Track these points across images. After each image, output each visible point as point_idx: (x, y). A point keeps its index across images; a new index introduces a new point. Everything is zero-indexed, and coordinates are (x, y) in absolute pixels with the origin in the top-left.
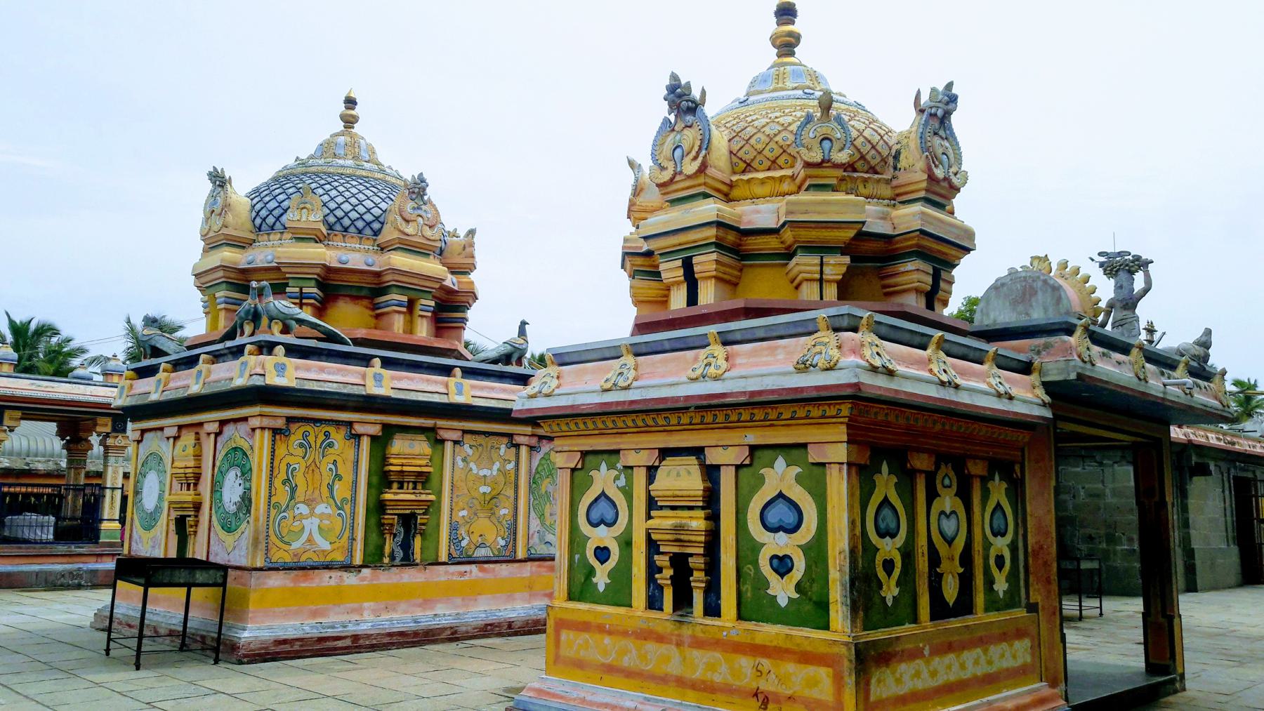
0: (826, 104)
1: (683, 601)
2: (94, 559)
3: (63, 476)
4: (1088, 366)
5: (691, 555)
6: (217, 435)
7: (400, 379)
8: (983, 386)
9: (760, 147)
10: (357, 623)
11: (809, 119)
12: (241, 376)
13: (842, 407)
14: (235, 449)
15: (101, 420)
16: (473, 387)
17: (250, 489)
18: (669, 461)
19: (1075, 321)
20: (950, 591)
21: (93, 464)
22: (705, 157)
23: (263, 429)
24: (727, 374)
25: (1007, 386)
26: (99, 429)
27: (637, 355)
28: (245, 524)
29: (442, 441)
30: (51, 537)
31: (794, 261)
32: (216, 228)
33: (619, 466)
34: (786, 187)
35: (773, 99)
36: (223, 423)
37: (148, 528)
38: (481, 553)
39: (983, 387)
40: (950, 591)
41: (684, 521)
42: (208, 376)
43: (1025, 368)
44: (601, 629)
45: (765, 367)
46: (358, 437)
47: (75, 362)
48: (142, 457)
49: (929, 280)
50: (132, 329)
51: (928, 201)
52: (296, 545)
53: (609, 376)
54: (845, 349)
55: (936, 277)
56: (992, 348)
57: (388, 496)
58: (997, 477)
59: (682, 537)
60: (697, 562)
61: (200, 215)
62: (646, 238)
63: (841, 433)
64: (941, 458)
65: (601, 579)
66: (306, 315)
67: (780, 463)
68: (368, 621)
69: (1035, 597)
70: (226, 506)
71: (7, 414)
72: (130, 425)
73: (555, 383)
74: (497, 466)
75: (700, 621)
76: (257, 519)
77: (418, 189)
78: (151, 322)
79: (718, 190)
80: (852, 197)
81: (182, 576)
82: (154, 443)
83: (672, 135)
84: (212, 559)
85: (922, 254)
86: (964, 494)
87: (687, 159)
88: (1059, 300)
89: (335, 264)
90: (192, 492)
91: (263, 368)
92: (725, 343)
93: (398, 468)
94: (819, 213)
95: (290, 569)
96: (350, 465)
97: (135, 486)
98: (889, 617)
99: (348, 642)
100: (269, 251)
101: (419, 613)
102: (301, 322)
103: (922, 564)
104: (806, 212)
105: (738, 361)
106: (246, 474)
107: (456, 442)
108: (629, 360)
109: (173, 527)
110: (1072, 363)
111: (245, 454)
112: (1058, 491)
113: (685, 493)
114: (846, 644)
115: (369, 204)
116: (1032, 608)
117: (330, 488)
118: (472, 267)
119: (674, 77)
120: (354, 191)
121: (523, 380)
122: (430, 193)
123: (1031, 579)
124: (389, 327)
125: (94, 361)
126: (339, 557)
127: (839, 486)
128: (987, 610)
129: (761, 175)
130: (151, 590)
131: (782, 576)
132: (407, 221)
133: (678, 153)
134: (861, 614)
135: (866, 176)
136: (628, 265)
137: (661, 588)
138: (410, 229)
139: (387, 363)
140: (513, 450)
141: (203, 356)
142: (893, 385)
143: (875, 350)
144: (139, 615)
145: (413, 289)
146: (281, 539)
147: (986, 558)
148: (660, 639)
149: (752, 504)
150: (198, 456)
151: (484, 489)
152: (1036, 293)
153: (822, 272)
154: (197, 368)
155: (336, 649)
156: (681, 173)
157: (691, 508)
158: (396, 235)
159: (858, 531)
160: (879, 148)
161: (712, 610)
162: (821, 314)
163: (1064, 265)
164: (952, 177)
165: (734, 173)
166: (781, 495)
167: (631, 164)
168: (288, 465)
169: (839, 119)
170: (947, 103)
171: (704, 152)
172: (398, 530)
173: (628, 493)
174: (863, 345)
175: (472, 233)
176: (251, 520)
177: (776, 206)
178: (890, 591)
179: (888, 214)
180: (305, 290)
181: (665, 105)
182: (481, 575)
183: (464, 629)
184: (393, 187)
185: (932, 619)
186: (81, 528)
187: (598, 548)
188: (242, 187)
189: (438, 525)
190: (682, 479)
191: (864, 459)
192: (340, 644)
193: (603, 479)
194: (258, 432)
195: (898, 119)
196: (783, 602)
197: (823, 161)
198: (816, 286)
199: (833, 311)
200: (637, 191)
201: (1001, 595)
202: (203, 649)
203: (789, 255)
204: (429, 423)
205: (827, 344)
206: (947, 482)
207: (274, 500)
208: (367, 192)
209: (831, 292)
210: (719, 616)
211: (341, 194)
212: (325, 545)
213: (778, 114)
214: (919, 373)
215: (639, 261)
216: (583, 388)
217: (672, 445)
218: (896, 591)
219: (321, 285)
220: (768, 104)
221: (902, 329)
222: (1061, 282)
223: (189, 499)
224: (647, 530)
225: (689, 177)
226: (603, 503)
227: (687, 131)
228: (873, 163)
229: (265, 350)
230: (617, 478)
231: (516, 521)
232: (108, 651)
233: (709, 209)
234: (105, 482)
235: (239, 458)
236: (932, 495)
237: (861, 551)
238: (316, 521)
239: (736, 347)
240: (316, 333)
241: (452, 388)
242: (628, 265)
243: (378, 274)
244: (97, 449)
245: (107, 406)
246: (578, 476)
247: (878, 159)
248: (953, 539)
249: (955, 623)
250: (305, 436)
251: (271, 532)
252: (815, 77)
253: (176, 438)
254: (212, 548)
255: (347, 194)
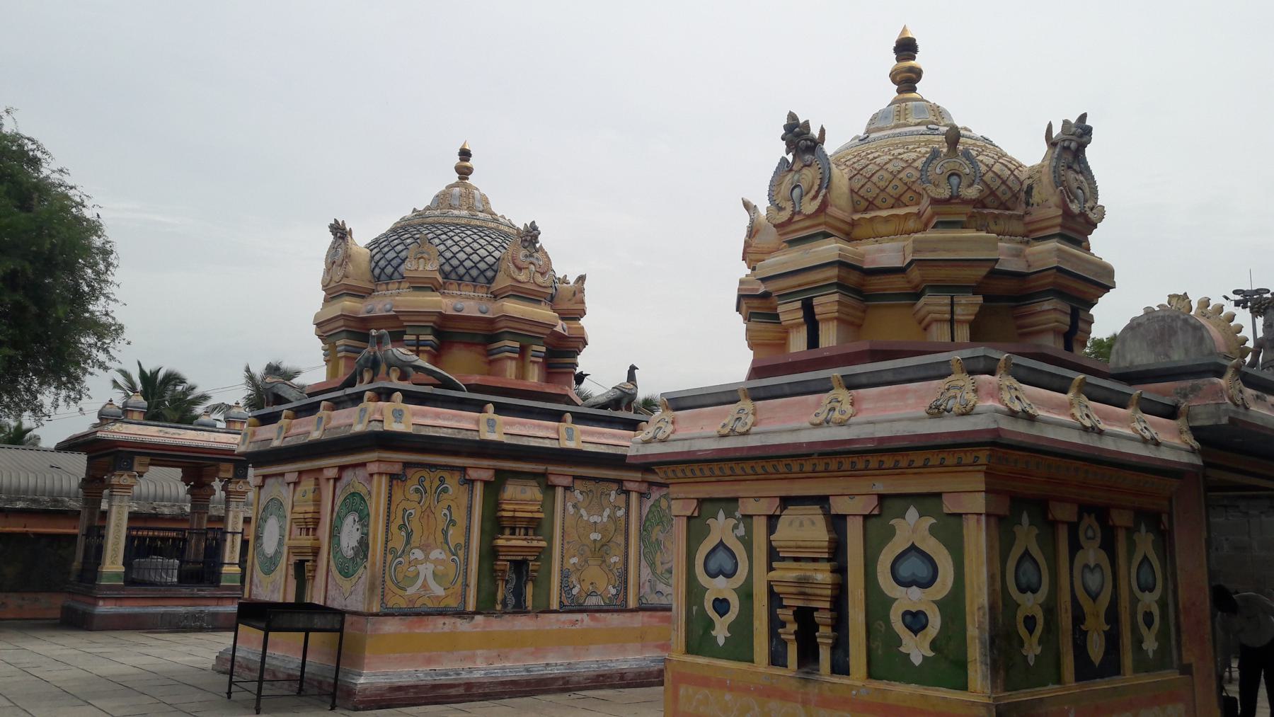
0: (954, 136)
1: (808, 655)
2: (214, 602)
3: (187, 521)
4: (1242, 410)
5: (817, 609)
6: (336, 480)
7: (512, 424)
8: (1128, 432)
9: (883, 184)
10: (470, 670)
11: (935, 154)
12: (361, 422)
13: (980, 454)
14: (353, 494)
15: (224, 466)
16: (583, 432)
17: (367, 534)
18: (791, 510)
19: (1225, 362)
20: (1096, 650)
21: (215, 509)
22: (825, 196)
23: (380, 474)
24: (853, 420)
25: (1153, 432)
26: (222, 475)
27: (755, 399)
28: (362, 569)
29: (554, 487)
30: (175, 580)
31: (923, 301)
32: (337, 278)
33: (738, 514)
34: (911, 224)
35: (894, 136)
36: (342, 468)
37: (268, 572)
38: (592, 601)
39: (1125, 430)
40: (1096, 650)
41: (809, 574)
42: (328, 423)
43: (1171, 413)
44: (721, 685)
45: (894, 411)
46: (471, 482)
47: (199, 410)
48: (263, 501)
49: (1068, 319)
50: (251, 377)
51: (1062, 237)
52: (411, 591)
53: (726, 421)
54: (982, 392)
55: (1075, 316)
56: (1136, 391)
57: (500, 542)
58: (1143, 528)
59: (807, 590)
60: (823, 617)
61: (322, 266)
62: (764, 280)
63: (979, 482)
64: (1085, 509)
65: (721, 633)
66: (423, 362)
67: (912, 513)
68: (480, 668)
69: (1188, 658)
70: (344, 550)
71: (137, 459)
72: (251, 471)
73: (670, 428)
74: (607, 512)
75: (828, 678)
76: (374, 564)
77: (530, 236)
78: (273, 370)
79: (839, 230)
80: (983, 234)
81: (301, 619)
82: (276, 489)
83: (790, 176)
84: (329, 604)
85: (1060, 293)
86: (1109, 546)
87: (806, 199)
88: (1201, 340)
89: (450, 312)
90: (311, 537)
91: (382, 414)
92: (850, 387)
93: (510, 514)
94: (948, 251)
95: (405, 615)
96: (464, 512)
97: (256, 530)
98: (1032, 677)
99: (461, 691)
100: (388, 300)
101: (531, 662)
102: (418, 369)
103: (1066, 620)
104: (934, 250)
105: (865, 406)
106: (364, 519)
107: (567, 488)
108: (747, 405)
109: (292, 572)
110: (1223, 407)
111: (363, 499)
112: (1209, 543)
113: (808, 544)
114: (986, 705)
115: (482, 252)
116: (1186, 670)
117: (445, 533)
118: (582, 313)
119: (792, 116)
120: (469, 240)
121: (633, 425)
122: (543, 240)
123: (1184, 638)
124: (501, 373)
125: (216, 408)
126: (453, 603)
127: (976, 538)
128: (1136, 670)
129: (884, 213)
130: (271, 634)
131: (916, 633)
132: (520, 269)
133: (797, 191)
134: (1002, 673)
135: (996, 212)
136: (744, 307)
137: (785, 643)
138: (522, 277)
139: (500, 409)
140: (623, 496)
141: (323, 403)
142: (1035, 431)
143: (1014, 393)
144: (258, 659)
145: (526, 334)
146: (397, 585)
147: (1133, 615)
148: (785, 696)
149: (881, 557)
150: (317, 502)
151: (594, 536)
152: (1176, 332)
153: (952, 312)
154: (318, 414)
155: (448, 697)
156: (799, 212)
157: (815, 560)
158: (509, 282)
159: (998, 586)
160: (1009, 183)
161: (840, 668)
162: (956, 356)
163: (1205, 303)
164: (1088, 212)
165: (856, 211)
166: (913, 548)
167: (747, 205)
168: (405, 510)
169: (966, 154)
170: (1081, 136)
171: (824, 191)
172: (510, 578)
173: (747, 542)
174: (1000, 389)
175: (582, 279)
176: (368, 565)
177: (902, 244)
178: (1032, 649)
179: (1021, 251)
180: (422, 338)
181: (783, 145)
182: (592, 624)
183: (576, 679)
184: (507, 235)
185: (1078, 679)
186: (203, 572)
187: (717, 599)
188: (362, 237)
189: (549, 572)
190: (806, 529)
191: (1003, 509)
192: (453, 692)
193: (721, 528)
194: (375, 477)
195: (1029, 152)
196: (917, 660)
197: (951, 197)
198: (947, 327)
199: (967, 353)
200: (753, 232)
201: (1151, 655)
202: (319, 695)
203: (916, 295)
204: (539, 468)
205: (962, 388)
206: (1090, 533)
207: (390, 545)
208: (481, 241)
209: (963, 334)
210: (847, 673)
211: (456, 243)
212: (439, 591)
213: (901, 151)
214: (1059, 416)
215: (756, 303)
216: (699, 433)
217: (794, 494)
218: (1038, 650)
219: (437, 332)
220: (890, 141)
221: (1041, 371)
222: (1203, 321)
223: (308, 543)
224: (769, 582)
225: (809, 217)
226: (721, 554)
227: (805, 171)
228: (1004, 198)
229: (383, 397)
230: (735, 527)
231: (626, 570)
232: (229, 693)
233: (830, 249)
234: (226, 527)
235: (356, 504)
236: (1075, 547)
237: (1001, 607)
238: (431, 567)
239: (861, 391)
240: (431, 379)
241: (562, 431)
242: (744, 307)
243: (491, 321)
244: (219, 494)
245: (231, 452)
246: (696, 528)
247: (1009, 194)
248: (1098, 594)
249: (1101, 685)
250: (421, 482)
251: (387, 577)
252: (938, 112)
253: (296, 484)
254: (330, 593)
255: (462, 243)
